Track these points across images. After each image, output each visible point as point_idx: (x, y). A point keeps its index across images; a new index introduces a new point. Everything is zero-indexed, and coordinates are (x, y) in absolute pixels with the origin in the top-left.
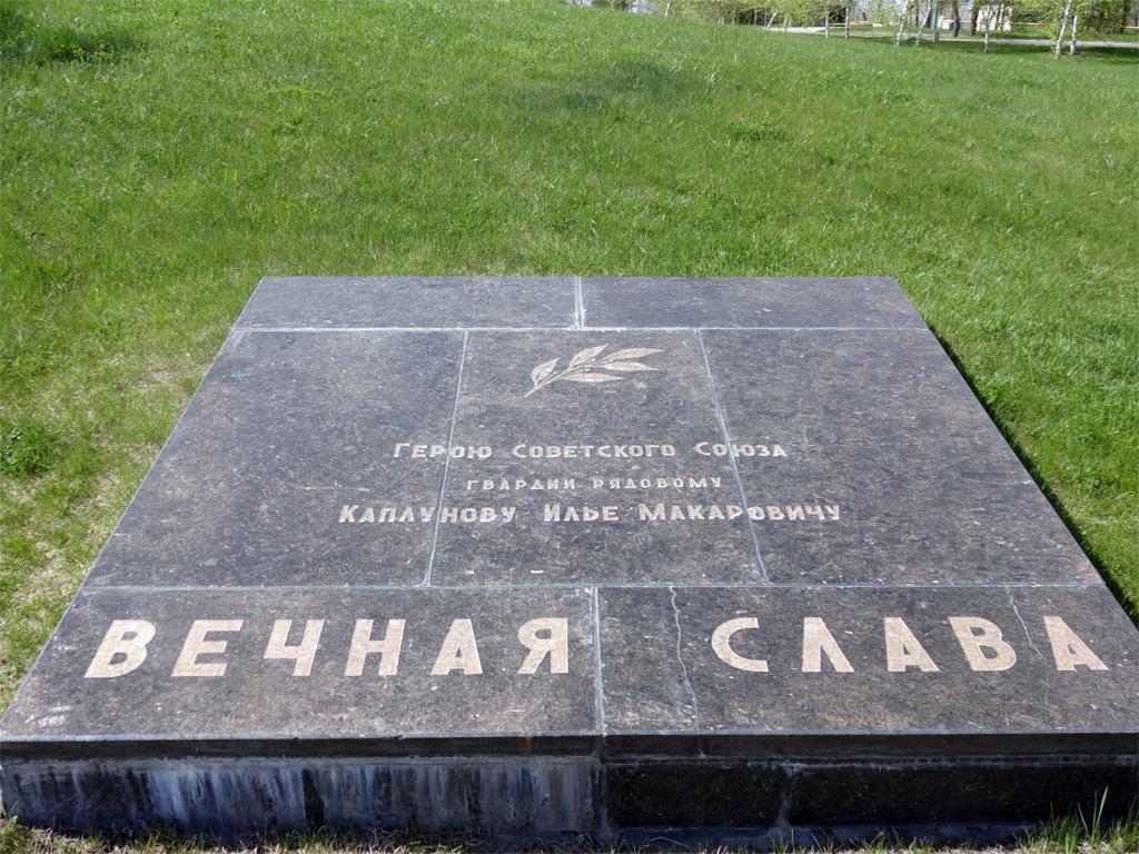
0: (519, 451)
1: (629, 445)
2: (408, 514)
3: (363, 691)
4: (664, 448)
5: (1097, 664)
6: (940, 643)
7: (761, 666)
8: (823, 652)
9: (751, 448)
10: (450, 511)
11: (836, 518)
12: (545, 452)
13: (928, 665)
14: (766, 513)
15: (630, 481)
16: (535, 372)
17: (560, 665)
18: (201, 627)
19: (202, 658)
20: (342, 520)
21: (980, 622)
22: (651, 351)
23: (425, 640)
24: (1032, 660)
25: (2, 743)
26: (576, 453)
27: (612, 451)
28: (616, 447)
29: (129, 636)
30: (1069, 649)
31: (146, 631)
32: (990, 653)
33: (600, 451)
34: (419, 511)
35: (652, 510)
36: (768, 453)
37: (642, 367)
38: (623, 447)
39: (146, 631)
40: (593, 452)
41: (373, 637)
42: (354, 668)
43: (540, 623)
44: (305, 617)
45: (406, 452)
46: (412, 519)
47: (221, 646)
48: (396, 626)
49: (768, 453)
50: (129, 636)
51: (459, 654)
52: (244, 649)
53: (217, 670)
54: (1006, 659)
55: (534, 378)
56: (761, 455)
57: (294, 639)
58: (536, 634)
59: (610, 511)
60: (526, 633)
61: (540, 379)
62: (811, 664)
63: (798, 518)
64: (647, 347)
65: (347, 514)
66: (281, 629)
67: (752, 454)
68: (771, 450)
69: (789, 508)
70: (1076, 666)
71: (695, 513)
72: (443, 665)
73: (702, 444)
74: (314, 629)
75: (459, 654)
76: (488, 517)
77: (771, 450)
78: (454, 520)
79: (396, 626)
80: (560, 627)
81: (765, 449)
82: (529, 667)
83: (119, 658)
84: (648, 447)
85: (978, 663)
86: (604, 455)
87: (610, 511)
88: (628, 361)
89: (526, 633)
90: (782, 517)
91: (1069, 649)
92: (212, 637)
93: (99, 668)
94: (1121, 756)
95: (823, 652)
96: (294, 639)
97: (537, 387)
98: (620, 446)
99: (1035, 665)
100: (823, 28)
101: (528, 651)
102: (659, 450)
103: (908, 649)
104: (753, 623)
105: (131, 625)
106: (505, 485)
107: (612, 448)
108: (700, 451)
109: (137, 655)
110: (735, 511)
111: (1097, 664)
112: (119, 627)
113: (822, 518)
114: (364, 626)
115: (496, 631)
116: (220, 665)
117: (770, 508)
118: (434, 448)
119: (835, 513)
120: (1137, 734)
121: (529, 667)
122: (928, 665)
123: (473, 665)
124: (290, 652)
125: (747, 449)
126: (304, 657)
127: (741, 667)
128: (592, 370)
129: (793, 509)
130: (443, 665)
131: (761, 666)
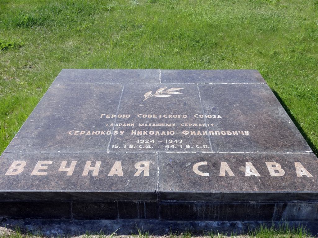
2: (150, 125)
5: (309, 175)
7: (207, 175)
9: (211, 116)
13: (257, 175)
17: (147, 174)
19: (40, 171)
22: (179, 89)
23: (107, 166)
24: (239, 85)
29: (19, 165)
30: (301, 171)
32: (277, 172)
34: (120, 132)
36: (215, 117)
37: (180, 93)
39: (24, 163)
42: (85, 173)
45: (104, 117)
47: (45, 168)
48: (98, 164)
49: (215, 117)
50: (19, 165)
51: (116, 171)
53: (45, 174)
54: (282, 173)
56: (214, 117)
57: (68, 165)
60: (138, 166)
62: (222, 174)
63: (236, 134)
64: (180, 88)
66: (64, 163)
67: (211, 117)
68: (217, 116)
70: (303, 175)
71: (158, 133)
72: (111, 174)
73: (196, 115)
74: (74, 163)
77: (217, 116)
81: (215, 116)
82: (137, 174)
83: (16, 170)
84: (179, 115)
85: (273, 174)
88: (174, 91)
89: (138, 166)
90: (231, 134)
93: (10, 172)
95: (226, 170)
96: (68, 165)
97: (146, 99)
99: (129, 173)
100: (276, 205)
105: (18, 162)
108: (195, 117)
109: (20, 170)
111: (309, 175)
114: (89, 163)
117: (227, 132)
119: (247, 133)
121: (137, 174)
122: (257, 175)
123: (120, 173)
126: (70, 171)
128: (163, 94)
129: (204, 132)
130: (111, 174)
131: (207, 175)
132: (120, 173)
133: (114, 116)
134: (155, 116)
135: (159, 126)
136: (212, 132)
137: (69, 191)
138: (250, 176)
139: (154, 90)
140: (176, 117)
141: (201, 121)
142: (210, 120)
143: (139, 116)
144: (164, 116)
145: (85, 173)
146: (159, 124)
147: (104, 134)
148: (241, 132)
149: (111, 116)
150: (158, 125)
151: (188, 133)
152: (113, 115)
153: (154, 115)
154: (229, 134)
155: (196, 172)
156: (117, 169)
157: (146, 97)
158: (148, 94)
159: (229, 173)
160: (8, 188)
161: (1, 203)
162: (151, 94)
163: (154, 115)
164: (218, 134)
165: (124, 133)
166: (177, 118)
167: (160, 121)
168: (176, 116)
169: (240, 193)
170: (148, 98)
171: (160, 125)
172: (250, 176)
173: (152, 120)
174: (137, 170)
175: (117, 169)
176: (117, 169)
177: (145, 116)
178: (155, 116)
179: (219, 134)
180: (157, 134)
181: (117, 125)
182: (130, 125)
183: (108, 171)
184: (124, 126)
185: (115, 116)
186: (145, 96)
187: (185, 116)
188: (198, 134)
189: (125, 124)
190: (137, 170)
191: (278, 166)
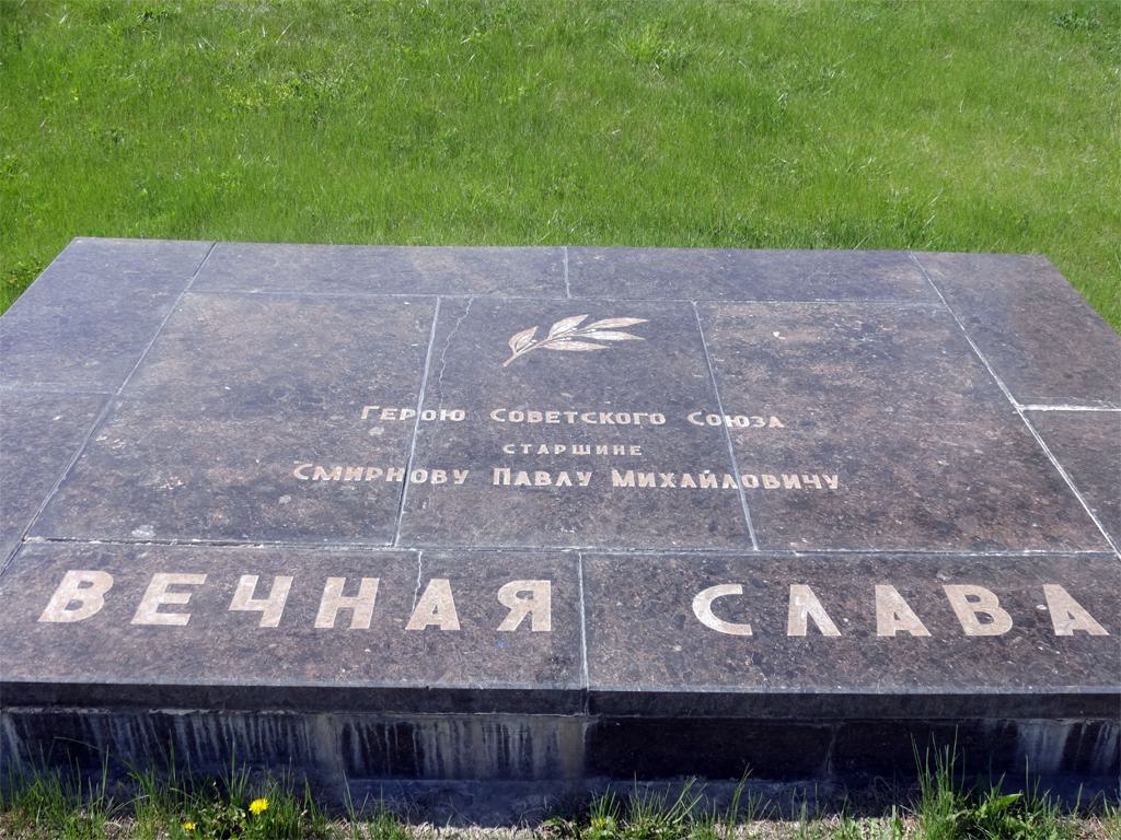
3: (342, 636)
5: (1096, 629)
7: (745, 630)
10: (396, 471)
12: (526, 417)
14: (761, 481)
15: (543, 446)
16: (555, 326)
17: (544, 624)
19: (163, 608)
20: (466, 472)
23: (397, 600)
25: (2, 683)
27: (597, 418)
28: (602, 415)
29: (85, 585)
31: (102, 581)
32: (983, 618)
33: (584, 417)
34: (452, 473)
38: (610, 414)
39: (102, 581)
40: (576, 418)
44: (360, 574)
46: (569, 484)
48: (369, 586)
52: (207, 607)
53: (182, 620)
54: (1002, 623)
55: (512, 346)
57: (262, 592)
60: (508, 592)
61: (518, 347)
62: (796, 628)
63: (789, 478)
66: (248, 582)
71: (542, 479)
72: (416, 623)
73: (497, 411)
74: (282, 587)
79: (369, 586)
80: (543, 589)
82: (511, 624)
83: (74, 605)
84: (636, 415)
85: (971, 627)
86: (498, 419)
88: (610, 331)
90: (777, 484)
91: (1067, 615)
96: (262, 592)
97: (516, 355)
98: (606, 413)
102: (648, 418)
104: (737, 590)
105: (89, 576)
106: (543, 449)
107: (598, 416)
108: (495, 418)
111: (1096, 629)
112: (72, 579)
113: (819, 487)
114: (334, 585)
115: (763, 602)
116: (240, 608)
118: (404, 411)
119: (834, 483)
120: (1119, 694)
121: (511, 624)
124: (259, 606)
125: (741, 420)
127: (712, 627)
128: (574, 339)
129: (789, 478)
131: (745, 630)
132: (451, 623)
134: (551, 417)
135: (582, 453)
136: (503, 470)
138: (1072, 634)
139: (544, 324)
140: (628, 421)
142: (624, 434)
144: (584, 417)
145: (325, 620)
148: (811, 478)
149: (398, 414)
150: (578, 450)
152: (404, 411)
153: (548, 414)
154: (771, 484)
156: (437, 606)
157: (514, 351)
158: (523, 341)
159: (816, 617)
160: (264, 670)
161: (1118, 716)
162: (533, 338)
163: (548, 414)
164: (502, 478)
165: (466, 480)
167: (577, 434)
168: (433, 413)
171: (585, 450)
173: (544, 432)
174: (505, 611)
175: (1070, 615)
176: (1070, 615)
177: (517, 416)
183: (405, 611)
185: (413, 413)
187: (657, 419)
188: (726, 486)
190: (505, 611)
191: (990, 601)
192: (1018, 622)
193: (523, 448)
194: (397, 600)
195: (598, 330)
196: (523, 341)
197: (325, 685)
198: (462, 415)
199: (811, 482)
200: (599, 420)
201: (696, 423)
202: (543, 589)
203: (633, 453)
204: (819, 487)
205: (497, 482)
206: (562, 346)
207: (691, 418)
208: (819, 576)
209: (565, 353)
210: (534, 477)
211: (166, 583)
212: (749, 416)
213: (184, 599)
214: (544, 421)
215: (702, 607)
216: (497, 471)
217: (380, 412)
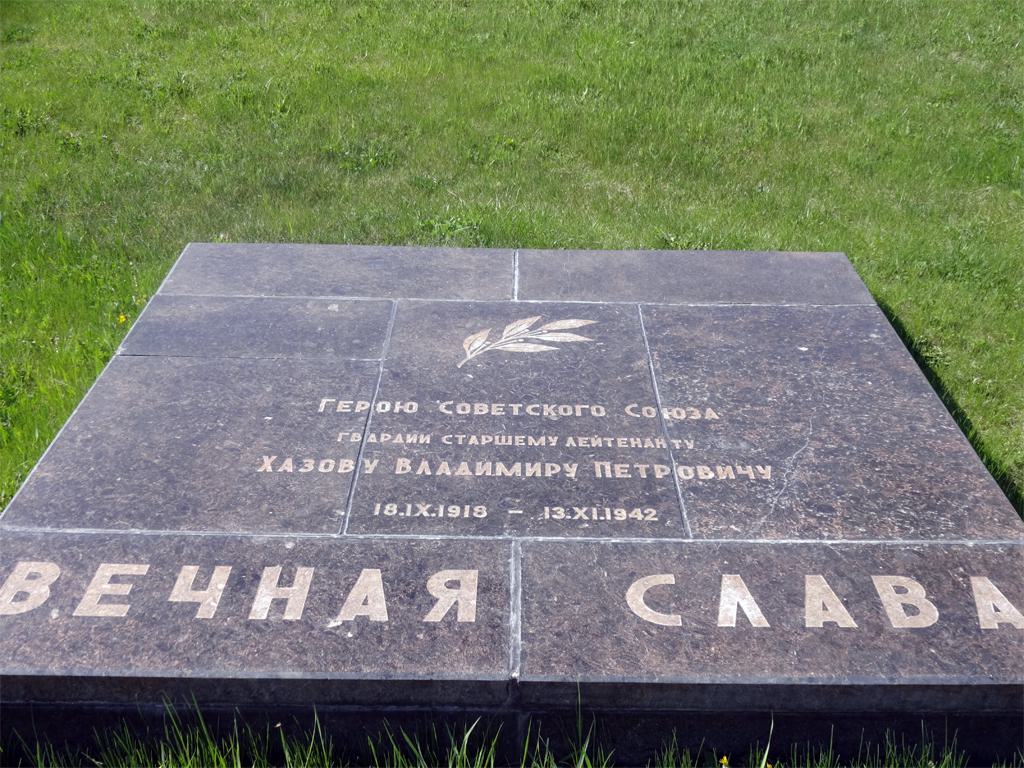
0: (533, 410)
1: (559, 404)
2: (473, 440)
4: (594, 408)
6: (861, 597)
7: (673, 620)
8: (739, 605)
11: (573, 475)
13: (846, 620)
17: (467, 614)
18: (106, 570)
19: (106, 599)
21: (903, 580)
25: (3, 676)
26: (504, 410)
27: (542, 410)
28: (545, 406)
29: (32, 577)
30: (992, 605)
31: (51, 571)
32: (911, 610)
33: (529, 409)
35: (509, 467)
37: (580, 338)
38: (553, 406)
39: (51, 571)
41: (280, 584)
43: (450, 574)
48: (304, 575)
50: (32, 577)
51: (825, 608)
53: (122, 611)
54: (929, 616)
55: (467, 349)
57: (200, 584)
58: (906, 591)
59: (621, 468)
61: (472, 349)
62: (726, 617)
65: (267, 465)
66: (189, 572)
67: (683, 416)
69: (409, 436)
70: (825, 623)
74: (221, 576)
75: (365, 603)
76: (481, 411)
78: (528, 465)
79: (304, 575)
82: (435, 616)
83: (21, 596)
84: (578, 408)
85: (898, 620)
87: (621, 468)
88: (563, 332)
89: (436, 583)
92: (115, 579)
94: (22, 702)
96: (200, 584)
97: (469, 357)
101: (29, 594)
102: (589, 410)
103: (370, 601)
104: (670, 579)
105: (33, 567)
108: (532, 413)
109: (40, 593)
110: (553, 468)
112: (24, 568)
114: (271, 574)
115: (407, 589)
117: (700, 469)
120: (1021, 686)
121: (435, 616)
122: (846, 620)
123: (379, 612)
126: (209, 602)
128: (526, 340)
132: (379, 612)
133: (363, 406)
135: (503, 442)
136: (603, 463)
137: (921, 677)
138: (821, 626)
140: (570, 413)
141: (656, 427)
143: (533, 410)
145: (261, 608)
146: (503, 437)
147: (270, 469)
149: (353, 407)
151: (666, 474)
155: (633, 607)
157: (468, 353)
158: (476, 344)
159: (749, 614)
163: (494, 406)
164: (603, 474)
166: (574, 415)
169: (933, 686)
170: (473, 355)
172: (821, 626)
174: (433, 602)
177: (464, 409)
178: (497, 410)
179: (609, 475)
180: (424, 472)
181: (375, 441)
182: (418, 440)
183: (333, 605)
184: (394, 441)
185: (368, 405)
186: (465, 346)
189: (474, 438)
190: (433, 602)
191: (917, 592)
192: (942, 617)
193: (457, 439)
194: (327, 599)
195: (549, 331)
196: (476, 344)
197: (707, 680)
198: (415, 406)
199: (744, 472)
200: (542, 413)
201: (535, 414)
202: (470, 577)
203: (620, 445)
204: (752, 476)
205: (599, 475)
206: (512, 347)
207: (628, 410)
208: (834, 566)
209: (513, 354)
210: (475, 467)
211: (109, 574)
212: (685, 409)
213: (126, 589)
214: (489, 413)
215: (635, 597)
216: (598, 465)
217: (337, 403)
